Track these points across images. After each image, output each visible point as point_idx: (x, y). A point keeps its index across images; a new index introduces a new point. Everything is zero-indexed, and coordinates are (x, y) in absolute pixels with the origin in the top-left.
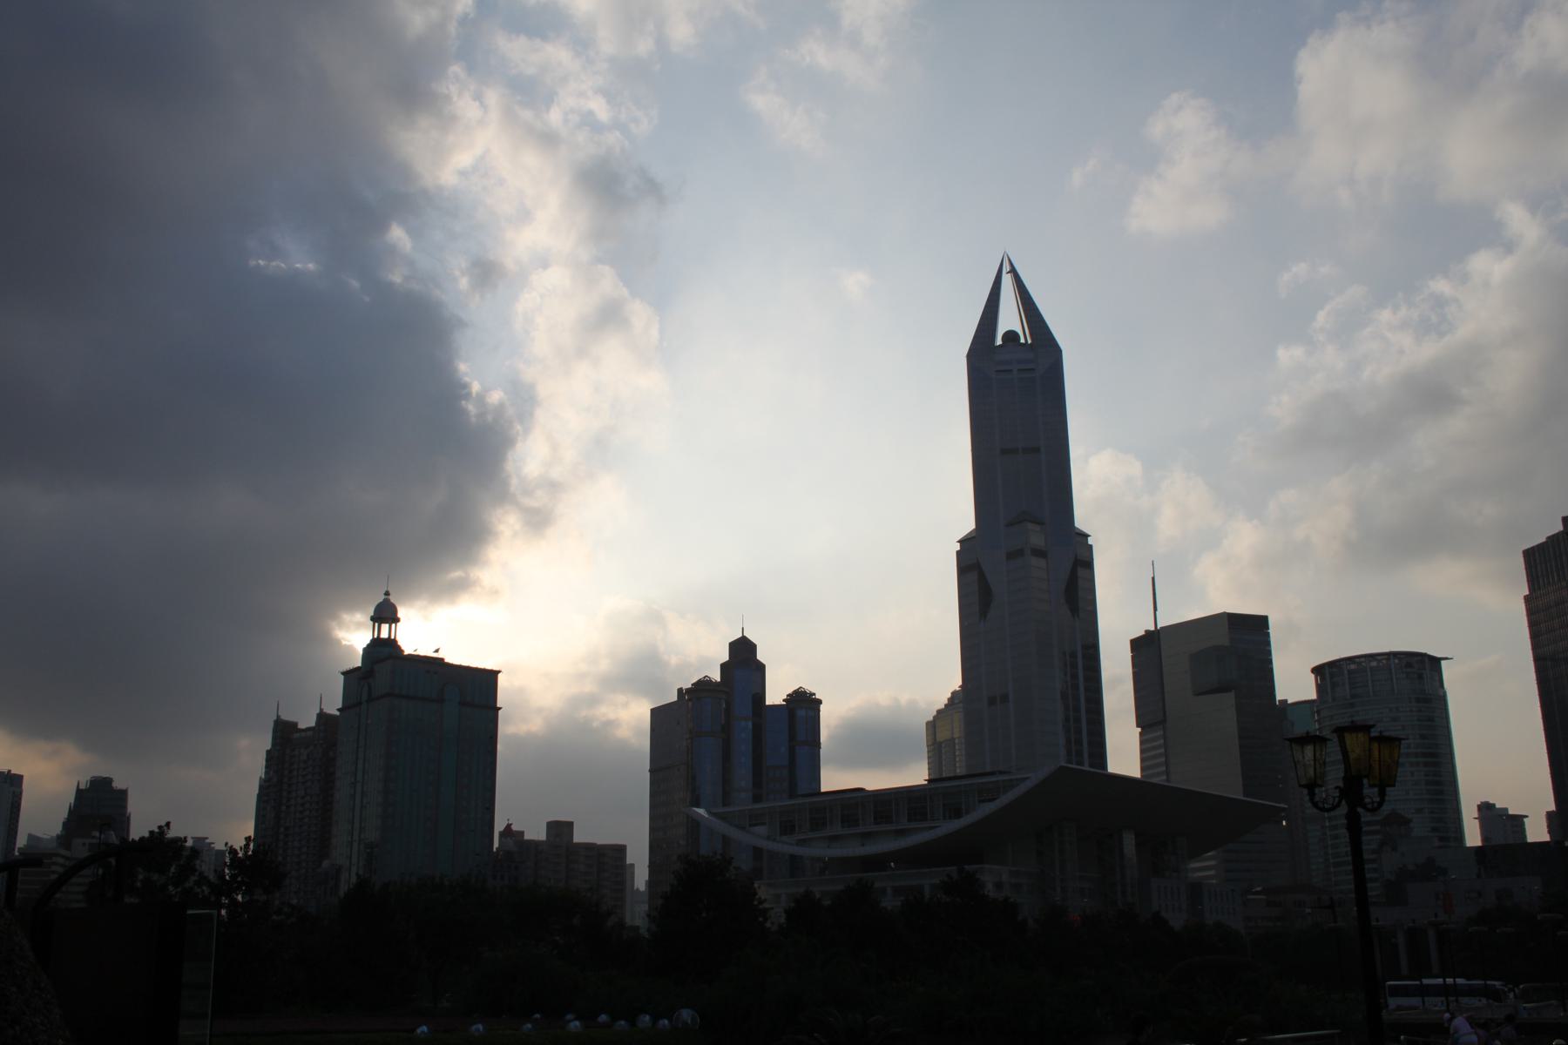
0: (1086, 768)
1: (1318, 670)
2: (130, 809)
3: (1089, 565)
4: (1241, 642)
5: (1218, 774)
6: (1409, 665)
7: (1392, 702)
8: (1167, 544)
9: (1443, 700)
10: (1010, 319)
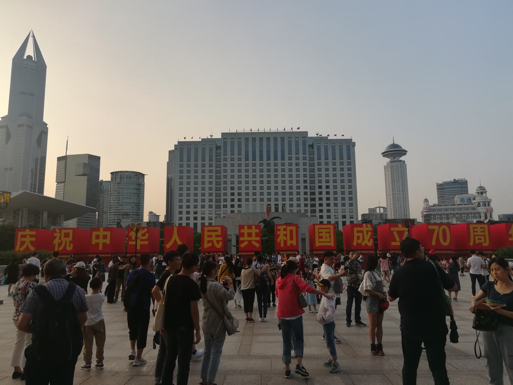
0: (36, 193)
1: (112, 173)
2: (197, 139)
3: (46, 133)
4: (93, 162)
5: (79, 198)
6: (136, 175)
7: (132, 182)
8: (66, 133)
9: (144, 185)
10: (30, 51)
